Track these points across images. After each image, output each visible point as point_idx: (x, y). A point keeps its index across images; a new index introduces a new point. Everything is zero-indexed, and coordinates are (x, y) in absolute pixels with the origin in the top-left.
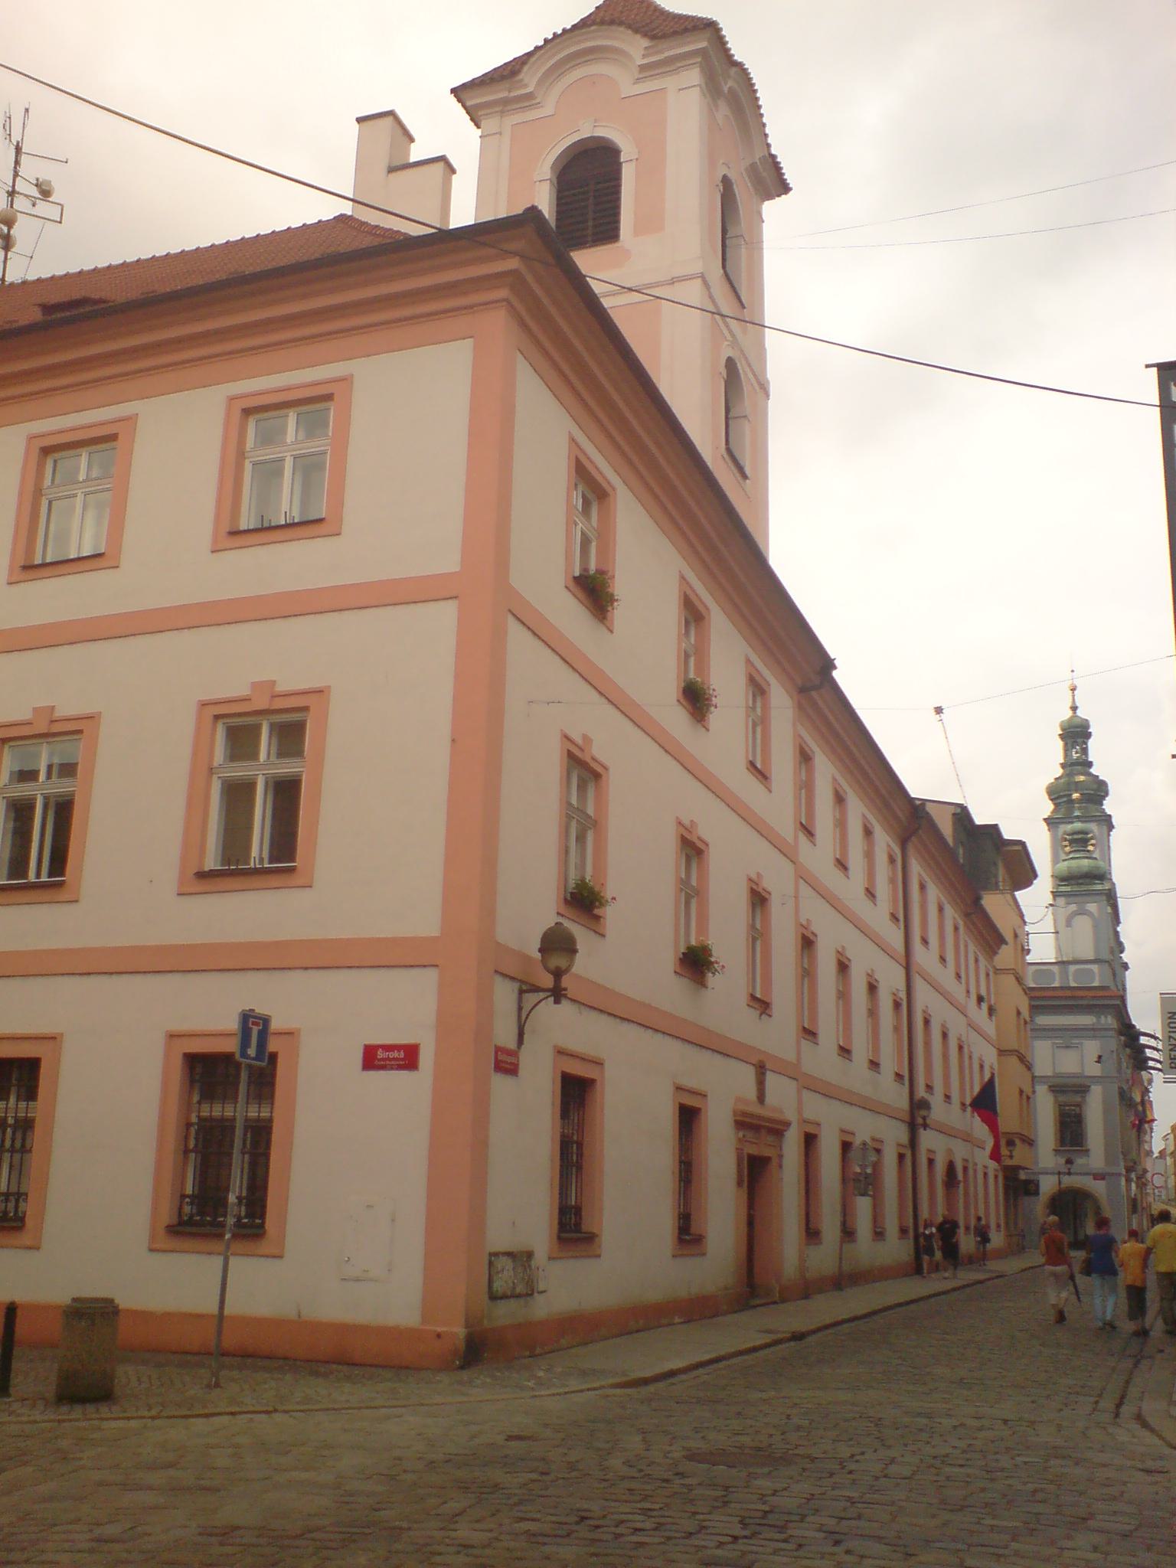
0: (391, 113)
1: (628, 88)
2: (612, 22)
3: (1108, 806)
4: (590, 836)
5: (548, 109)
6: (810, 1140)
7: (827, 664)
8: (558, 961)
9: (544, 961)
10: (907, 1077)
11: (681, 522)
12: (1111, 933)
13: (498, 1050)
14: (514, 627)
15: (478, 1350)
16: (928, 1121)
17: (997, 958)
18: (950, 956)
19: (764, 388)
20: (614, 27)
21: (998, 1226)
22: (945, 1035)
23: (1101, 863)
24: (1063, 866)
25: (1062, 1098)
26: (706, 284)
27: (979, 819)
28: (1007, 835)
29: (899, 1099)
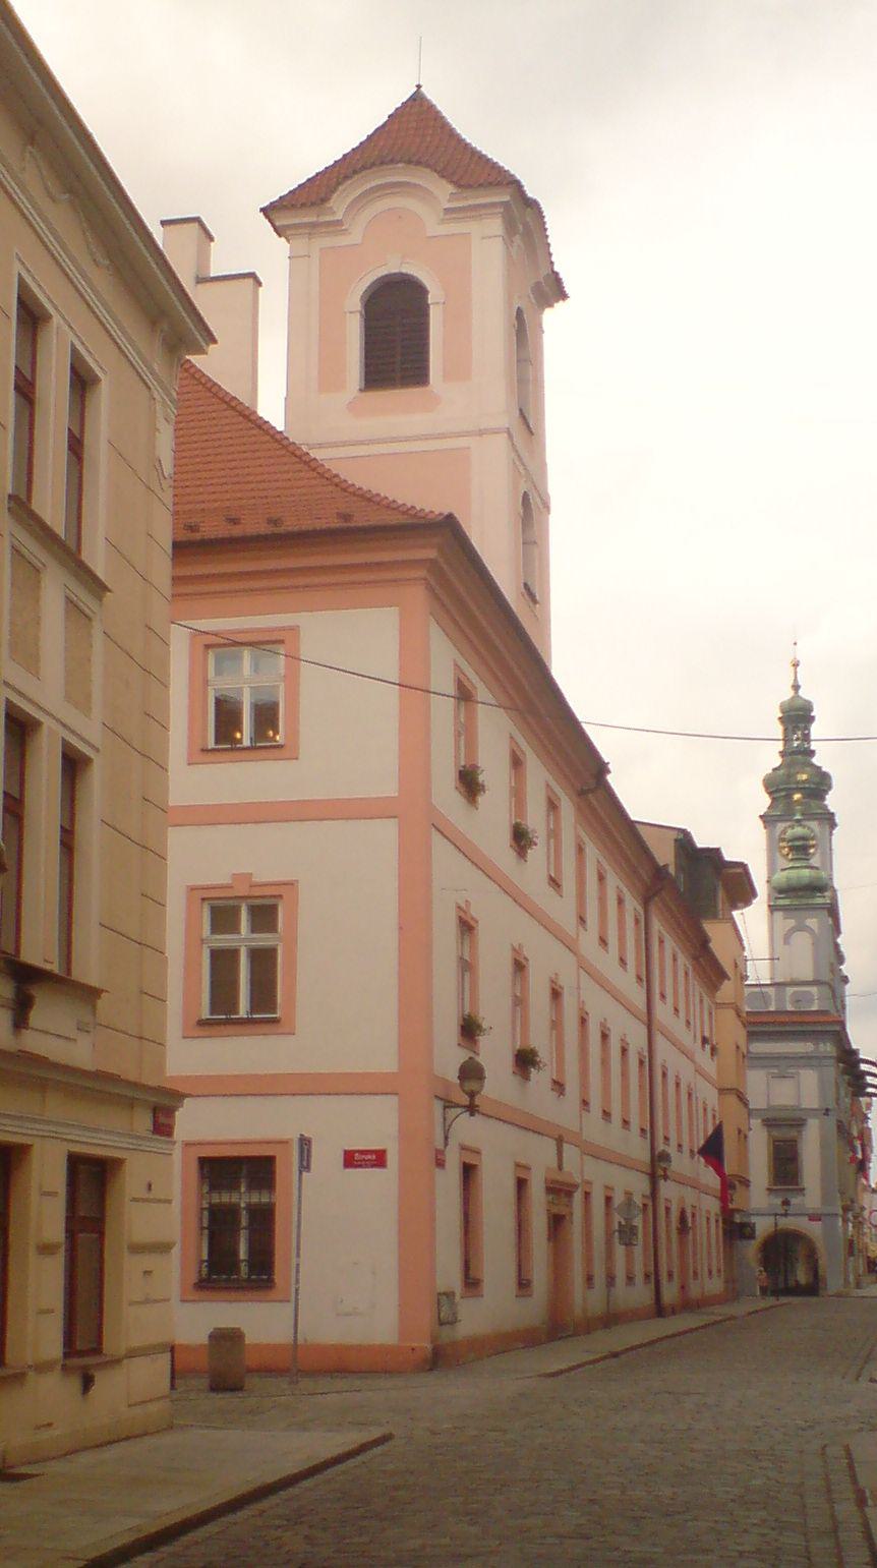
0: (197, 220)
1: (434, 226)
2: (418, 163)
3: (831, 801)
4: (467, 975)
5: (355, 236)
6: (587, 1195)
7: (601, 769)
8: (472, 1085)
9: (461, 1085)
10: (650, 1132)
11: (467, 630)
12: (832, 945)
13: (436, 1150)
14: (436, 837)
15: (439, 1358)
16: (669, 1173)
17: (718, 994)
18: (682, 1007)
19: (547, 507)
20: (419, 167)
21: (719, 1271)
22: (605, 1036)
23: (823, 874)
24: (781, 877)
25: (776, 1133)
26: (510, 436)
27: (701, 842)
28: (728, 856)
29: (639, 1151)
